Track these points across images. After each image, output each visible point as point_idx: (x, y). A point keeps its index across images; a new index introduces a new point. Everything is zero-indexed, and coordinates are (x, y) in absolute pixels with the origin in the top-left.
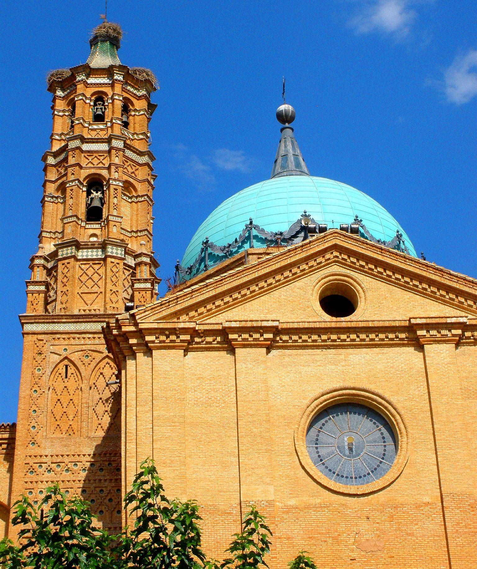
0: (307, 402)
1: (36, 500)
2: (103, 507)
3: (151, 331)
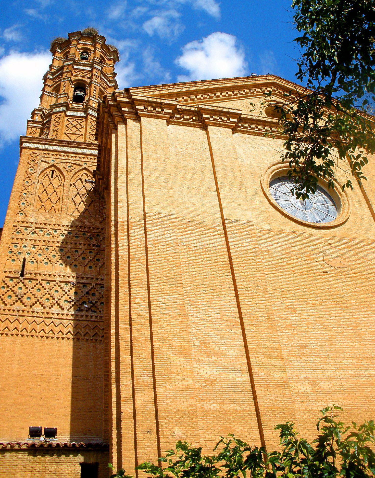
0: (266, 166)
1: (20, 251)
2: (77, 263)
3: (141, 102)
